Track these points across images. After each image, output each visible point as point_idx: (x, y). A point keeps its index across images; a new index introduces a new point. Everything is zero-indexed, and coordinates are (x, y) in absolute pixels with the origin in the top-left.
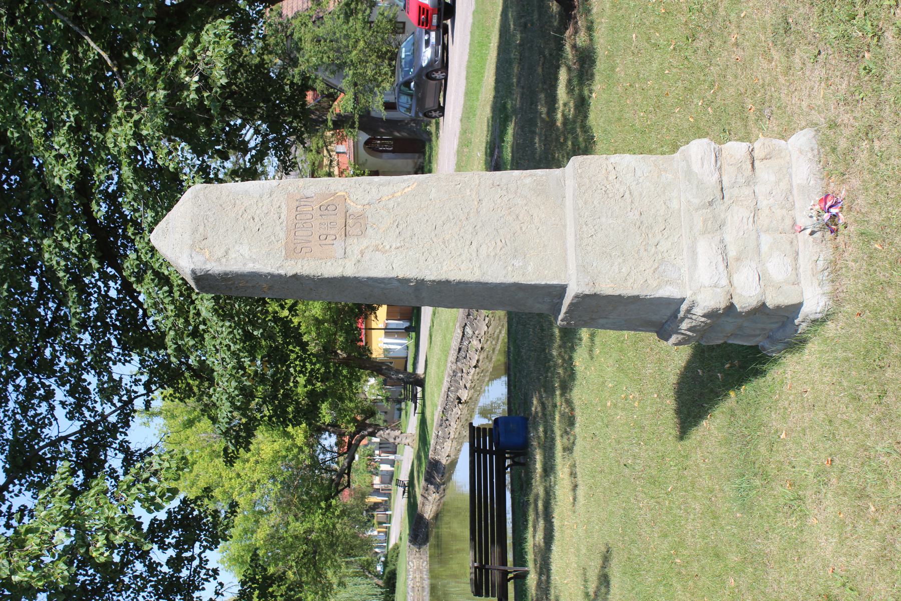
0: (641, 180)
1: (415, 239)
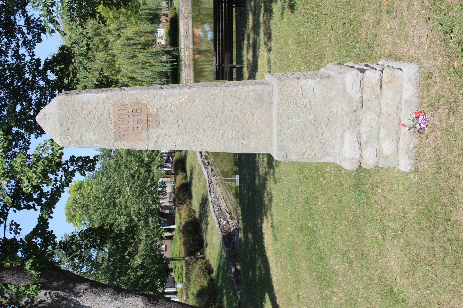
0: (316, 96)
1: (187, 129)
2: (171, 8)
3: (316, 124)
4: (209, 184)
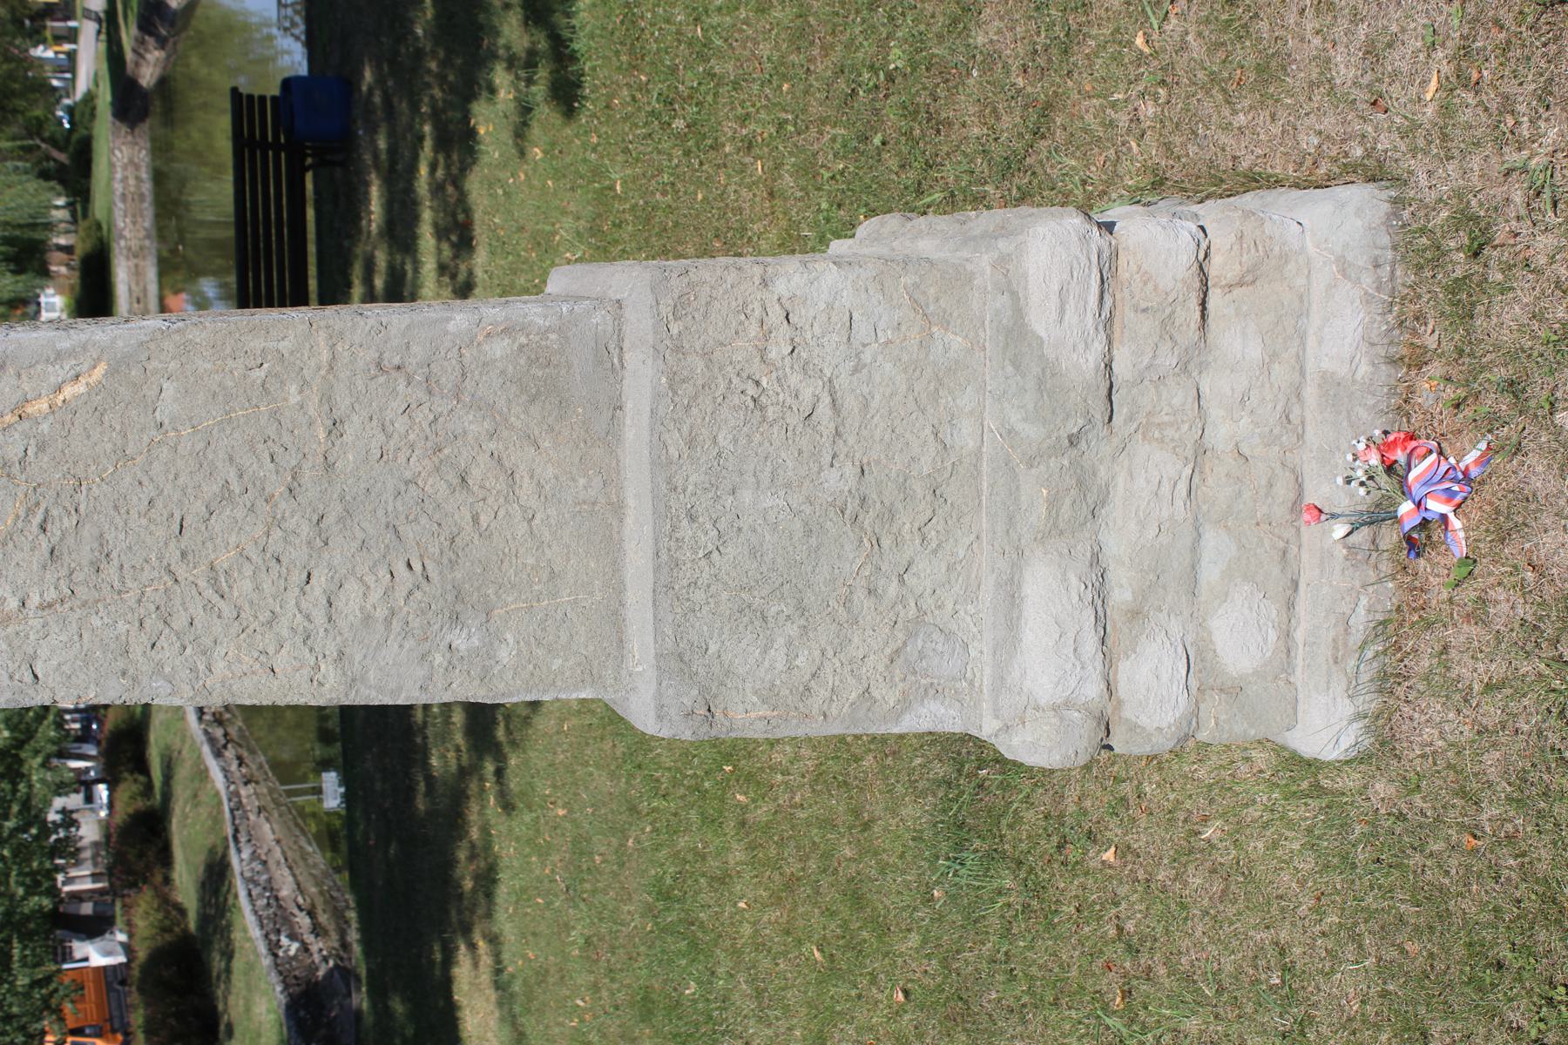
0: (867, 357)
1: (111, 572)
2: (83, 224)
3: (867, 521)
4: (232, 811)
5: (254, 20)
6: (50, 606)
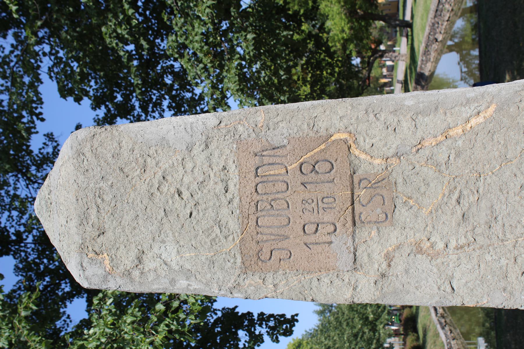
1: (497, 228)
5: (451, 81)
6: (462, 247)
